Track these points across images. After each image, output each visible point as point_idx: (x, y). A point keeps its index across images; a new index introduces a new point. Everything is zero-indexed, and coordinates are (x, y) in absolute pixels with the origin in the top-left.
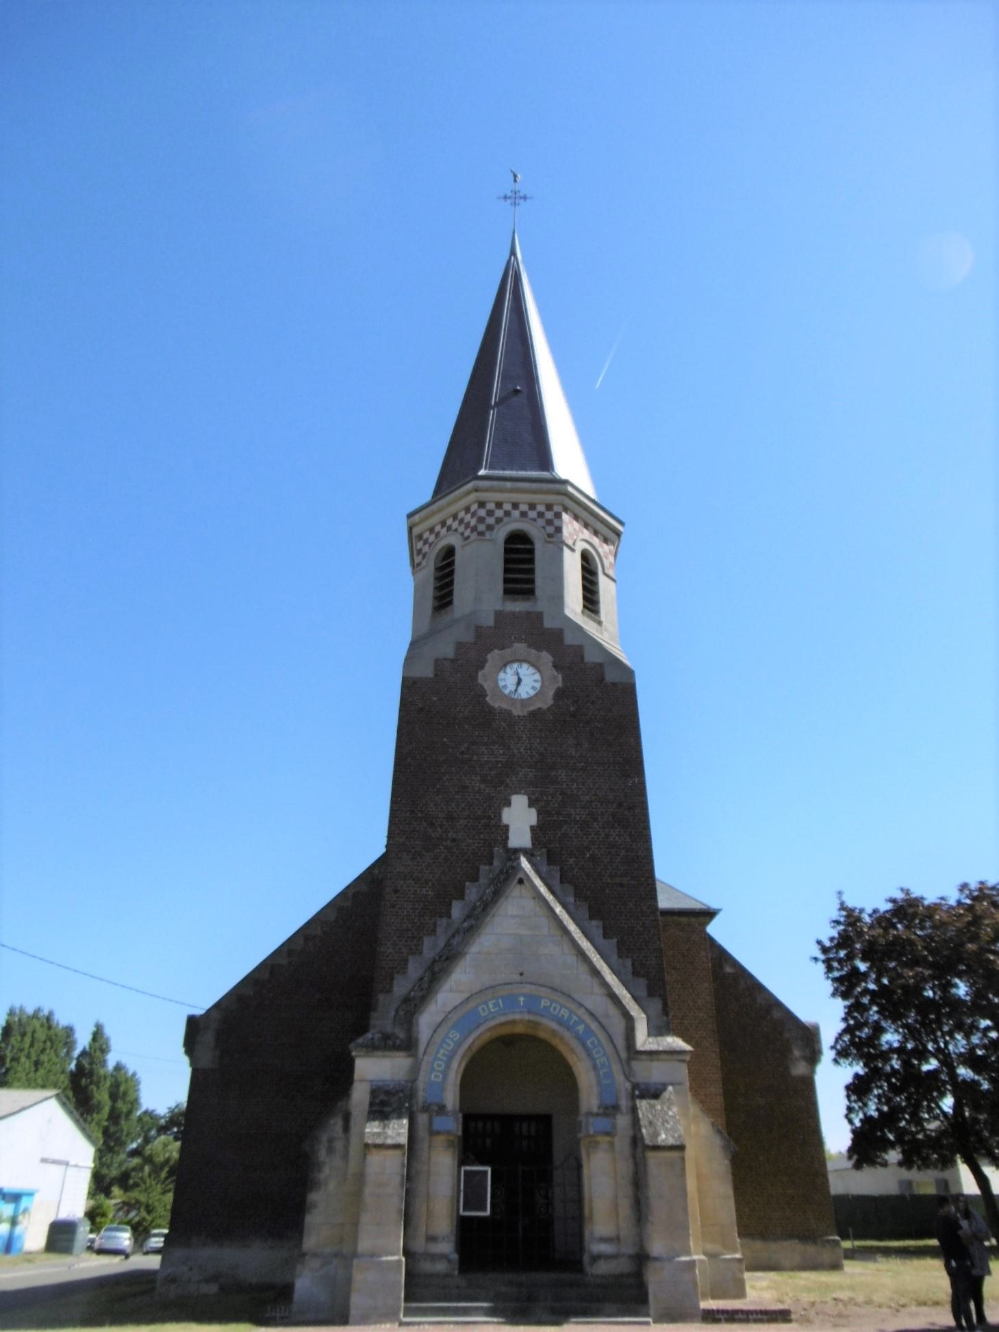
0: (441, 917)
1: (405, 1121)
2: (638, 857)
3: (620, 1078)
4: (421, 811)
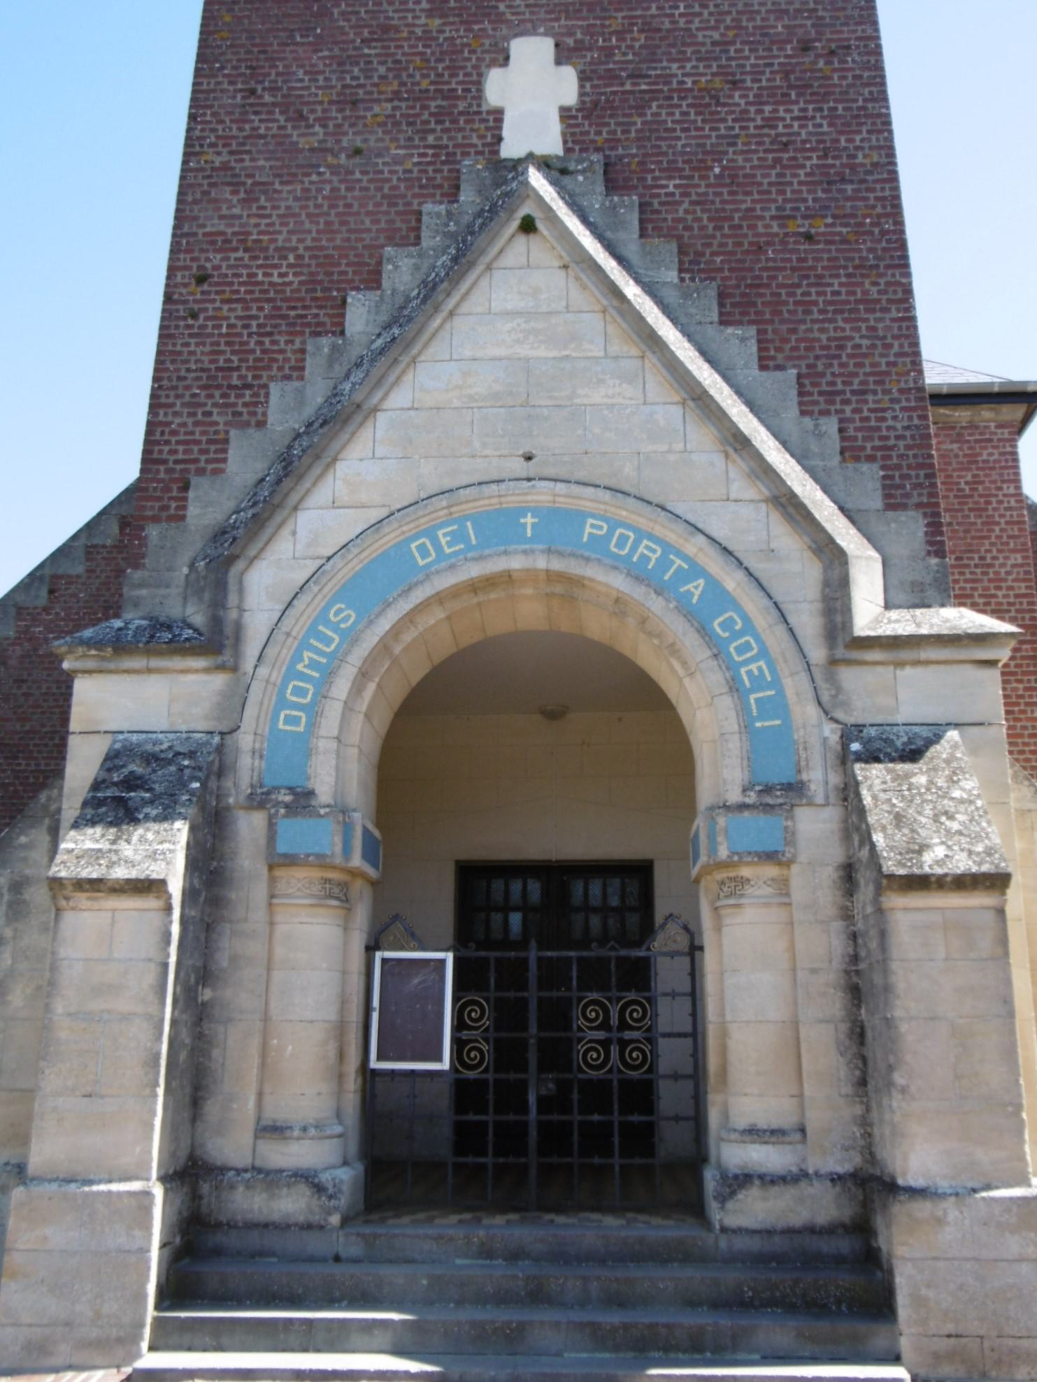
0: (317, 334)
1: (181, 830)
2: (853, 167)
3: (806, 713)
4: (273, 90)
